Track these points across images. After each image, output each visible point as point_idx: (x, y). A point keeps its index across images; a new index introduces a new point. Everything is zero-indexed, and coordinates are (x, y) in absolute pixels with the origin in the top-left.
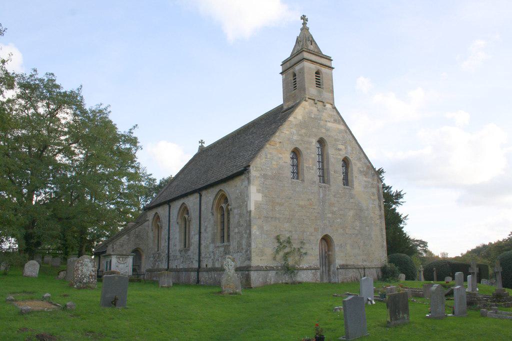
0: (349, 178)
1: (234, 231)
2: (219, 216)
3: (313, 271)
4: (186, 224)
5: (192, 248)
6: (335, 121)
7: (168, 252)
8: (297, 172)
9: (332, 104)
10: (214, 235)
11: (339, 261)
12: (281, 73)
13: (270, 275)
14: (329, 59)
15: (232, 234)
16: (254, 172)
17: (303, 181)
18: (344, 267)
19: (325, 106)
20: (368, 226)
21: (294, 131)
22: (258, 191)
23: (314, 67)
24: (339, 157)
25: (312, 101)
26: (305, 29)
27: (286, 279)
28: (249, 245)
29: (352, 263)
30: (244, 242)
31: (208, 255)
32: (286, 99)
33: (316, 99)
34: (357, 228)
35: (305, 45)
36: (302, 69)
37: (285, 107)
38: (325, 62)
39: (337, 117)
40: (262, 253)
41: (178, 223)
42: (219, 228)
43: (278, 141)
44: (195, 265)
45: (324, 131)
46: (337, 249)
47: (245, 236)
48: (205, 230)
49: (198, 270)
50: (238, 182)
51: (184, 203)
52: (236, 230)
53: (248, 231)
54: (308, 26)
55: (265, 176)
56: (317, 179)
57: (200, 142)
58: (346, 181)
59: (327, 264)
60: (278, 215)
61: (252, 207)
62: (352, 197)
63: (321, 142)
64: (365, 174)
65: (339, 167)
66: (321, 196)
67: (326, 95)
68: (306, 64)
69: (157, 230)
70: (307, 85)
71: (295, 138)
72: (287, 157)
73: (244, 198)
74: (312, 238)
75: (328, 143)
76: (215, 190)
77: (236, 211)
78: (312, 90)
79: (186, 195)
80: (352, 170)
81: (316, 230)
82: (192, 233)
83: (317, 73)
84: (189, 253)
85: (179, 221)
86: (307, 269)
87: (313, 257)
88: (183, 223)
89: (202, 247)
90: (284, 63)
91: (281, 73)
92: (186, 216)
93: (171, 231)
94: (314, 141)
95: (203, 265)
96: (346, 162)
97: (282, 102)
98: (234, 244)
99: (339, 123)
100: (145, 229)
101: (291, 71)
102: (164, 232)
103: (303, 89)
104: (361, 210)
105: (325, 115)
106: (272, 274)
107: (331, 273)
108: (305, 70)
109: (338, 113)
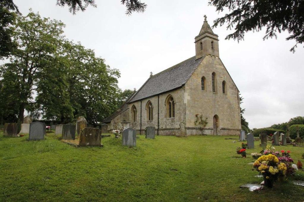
1: (176, 112)
2: (168, 106)
3: (211, 130)
4: (134, 113)
5: (154, 120)
6: (219, 64)
9: (218, 57)
10: (166, 114)
11: (221, 126)
12: (195, 42)
13: (193, 131)
14: (217, 36)
15: (175, 113)
16: (186, 87)
18: (223, 129)
19: (215, 58)
20: (233, 111)
21: (203, 69)
22: (188, 95)
23: (211, 40)
24: (221, 81)
25: (210, 56)
27: (200, 132)
28: (185, 118)
29: (226, 127)
30: (182, 117)
31: (163, 123)
32: (197, 54)
33: (212, 54)
34: (229, 112)
37: (197, 58)
39: (220, 63)
40: (190, 122)
41: (146, 109)
42: (168, 111)
43: (196, 73)
44: (157, 128)
45: (215, 69)
46: (220, 121)
47: (183, 114)
49: (158, 130)
50: (179, 92)
51: (149, 101)
53: (184, 112)
54: (207, 20)
55: (191, 89)
56: (212, 90)
59: (216, 127)
60: (196, 106)
61: (186, 102)
62: (227, 98)
63: (214, 74)
64: (232, 88)
65: (221, 85)
66: (214, 98)
67: (216, 52)
68: (207, 38)
69: (134, 113)
71: (203, 72)
72: (200, 80)
73: (182, 98)
74: (210, 116)
77: (177, 104)
81: (212, 112)
82: (154, 113)
83: (212, 42)
84: (153, 122)
85: (147, 108)
86: (208, 129)
87: (210, 124)
88: (148, 109)
89: (160, 120)
90: (196, 38)
91: (195, 42)
92: (150, 106)
93: (142, 113)
94: (211, 73)
95: (160, 127)
96: (224, 83)
98: (176, 118)
99: (221, 65)
100: (127, 112)
101: (200, 42)
102: (138, 114)
104: (230, 104)
105: (215, 62)
106: (194, 131)
107: (217, 131)
109: (221, 61)
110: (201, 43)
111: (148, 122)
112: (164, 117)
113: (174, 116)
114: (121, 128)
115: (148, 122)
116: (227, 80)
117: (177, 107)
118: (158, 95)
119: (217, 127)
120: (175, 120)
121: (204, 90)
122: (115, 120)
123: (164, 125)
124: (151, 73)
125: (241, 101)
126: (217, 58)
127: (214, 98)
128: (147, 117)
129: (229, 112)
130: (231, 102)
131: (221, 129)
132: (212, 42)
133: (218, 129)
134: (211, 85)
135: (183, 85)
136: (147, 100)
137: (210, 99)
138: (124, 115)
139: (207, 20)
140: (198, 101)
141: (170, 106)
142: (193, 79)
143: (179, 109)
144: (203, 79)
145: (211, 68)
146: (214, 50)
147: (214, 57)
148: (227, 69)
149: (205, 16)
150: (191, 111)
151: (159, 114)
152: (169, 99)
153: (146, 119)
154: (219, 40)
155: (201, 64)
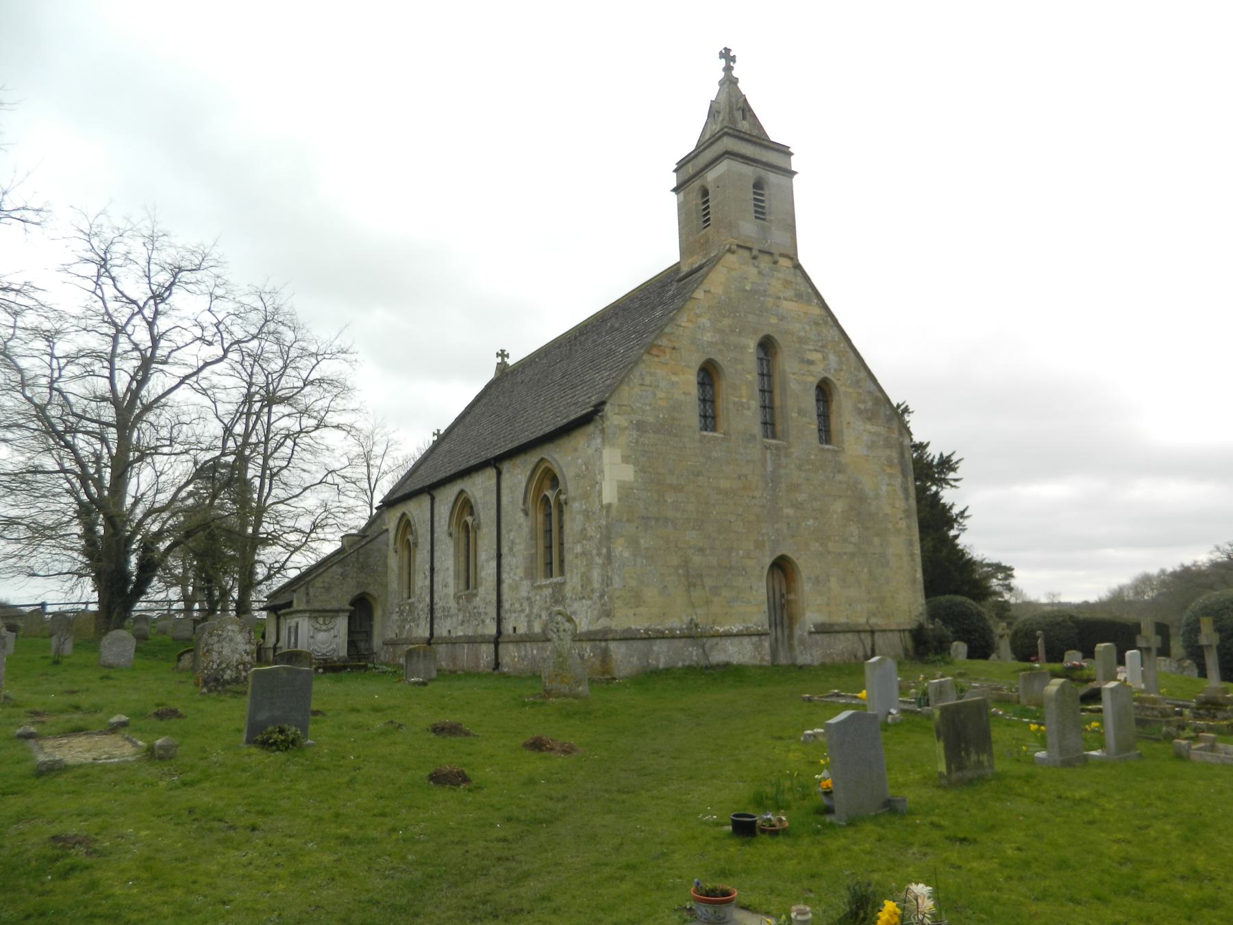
1: (573, 549)
3: (755, 639)
5: (481, 590)
6: (799, 296)
9: (792, 257)
10: (533, 558)
11: (812, 614)
14: (785, 151)
15: (568, 557)
16: (613, 417)
18: (824, 629)
19: (775, 262)
20: (878, 535)
23: (748, 171)
24: (810, 379)
25: (746, 254)
26: (729, 82)
28: (607, 581)
29: (843, 620)
30: (596, 574)
31: (517, 605)
32: (685, 250)
33: (756, 247)
37: (685, 269)
42: (541, 543)
43: (670, 345)
45: (774, 320)
47: (599, 560)
48: (511, 549)
51: (462, 492)
52: (578, 549)
53: (604, 551)
55: (640, 426)
56: (757, 429)
57: (498, 355)
59: (786, 623)
63: (767, 346)
64: (871, 417)
65: (809, 401)
66: (769, 468)
71: (708, 337)
72: (690, 380)
73: (592, 478)
77: (576, 505)
81: (759, 545)
82: (483, 556)
83: (758, 185)
85: (454, 530)
88: (462, 535)
90: (681, 166)
92: (469, 519)
93: (436, 554)
94: (752, 345)
95: (508, 628)
96: (824, 391)
98: (573, 581)
99: (809, 301)
101: (696, 184)
102: (422, 556)
104: (862, 498)
105: (775, 286)
107: (796, 642)
110: (705, 193)
111: (457, 598)
112: (520, 572)
113: (562, 572)
114: (237, 656)
115: (460, 597)
116: (842, 373)
117: (573, 524)
118: (496, 462)
119: (792, 620)
120: (568, 589)
121: (714, 429)
122: (311, 591)
123: (523, 617)
124: (502, 354)
125: (951, 475)
126: (784, 262)
127: (769, 468)
128: (457, 576)
129: (854, 540)
130: (867, 484)
131: (810, 633)
132: (758, 185)
133: (798, 632)
134: (755, 404)
135: (599, 408)
136: (532, 458)
137: (746, 476)
138: (363, 568)
139: (735, 73)
140: (677, 489)
141: (548, 516)
142: (652, 374)
143: (583, 536)
144: (709, 374)
145: (750, 318)
146: (770, 221)
147: (767, 258)
148: (840, 322)
149: (726, 55)
150: (642, 541)
151: (504, 561)
152: (541, 481)
153: (451, 582)
154: (794, 173)
155: (699, 294)
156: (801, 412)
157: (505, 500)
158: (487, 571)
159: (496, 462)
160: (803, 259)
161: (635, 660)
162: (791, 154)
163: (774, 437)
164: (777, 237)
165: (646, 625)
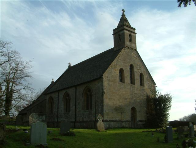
0: (142, 82)
5: (71, 112)
7: (58, 114)
8: (122, 79)
9: (136, 50)
13: (111, 124)
14: (134, 29)
17: (124, 83)
23: (128, 32)
26: (123, 15)
31: (80, 115)
35: (124, 22)
36: (124, 33)
37: (115, 50)
38: (132, 31)
47: (100, 106)
51: (66, 92)
57: (69, 64)
58: (142, 84)
63: (132, 67)
66: (132, 90)
70: (126, 40)
72: (118, 73)
75: (134, 67)
76: (65, 91)
78: (128, 43)
79: (68, 88)
80: (144, 79)
82: (71, 105)
83: (130, 35)
90: (114, 30)
91: (113, 35)
92: (52, 101)
95: (78, 119)
96: (141, 76)
97: (112, 46)
102: (55, 105)
103: (124, 42)
108: (124, 33)
118: (76, 86)
144: (121, 71)
149: (123, 10)
156: (137, 79)
157: (77, 94)
158: (73, 108)
159: (76, 86)
160: (138, 50)
161: (107, 126)
162: (135, 30)
163: (121, 82)
164: (133, 45)
165: (109, 119)
